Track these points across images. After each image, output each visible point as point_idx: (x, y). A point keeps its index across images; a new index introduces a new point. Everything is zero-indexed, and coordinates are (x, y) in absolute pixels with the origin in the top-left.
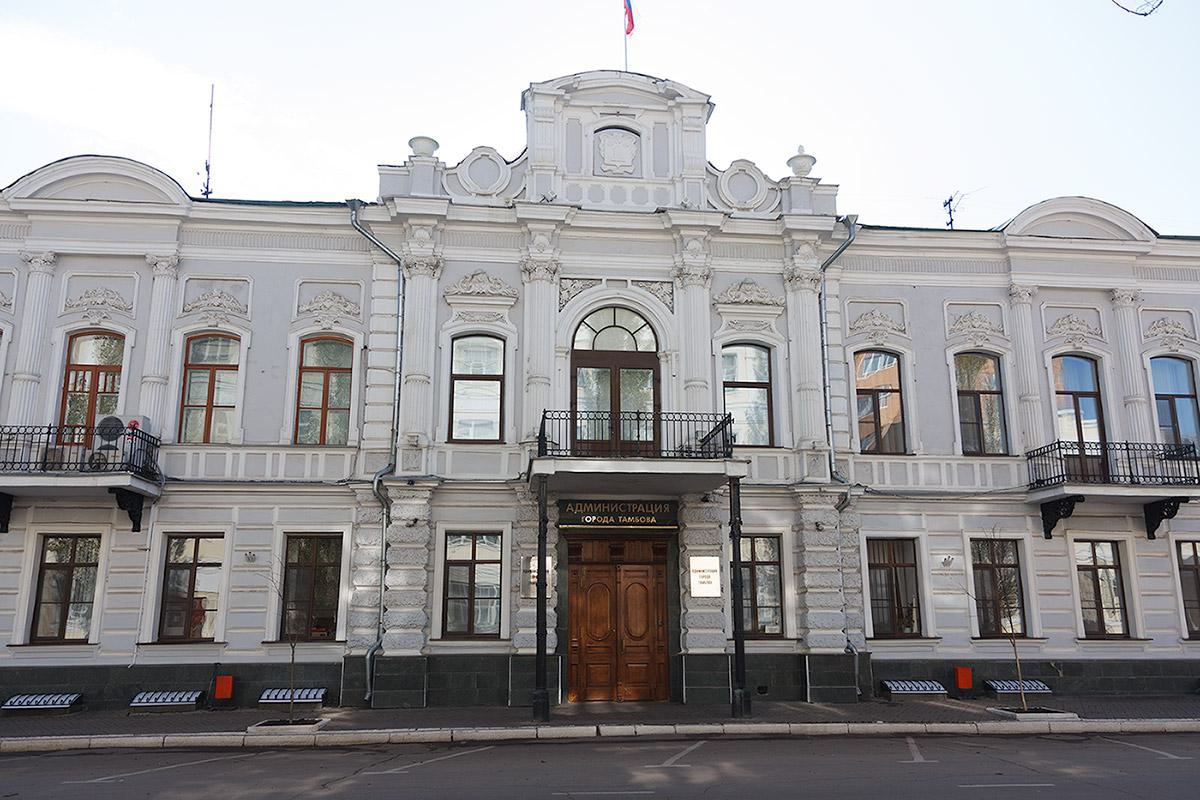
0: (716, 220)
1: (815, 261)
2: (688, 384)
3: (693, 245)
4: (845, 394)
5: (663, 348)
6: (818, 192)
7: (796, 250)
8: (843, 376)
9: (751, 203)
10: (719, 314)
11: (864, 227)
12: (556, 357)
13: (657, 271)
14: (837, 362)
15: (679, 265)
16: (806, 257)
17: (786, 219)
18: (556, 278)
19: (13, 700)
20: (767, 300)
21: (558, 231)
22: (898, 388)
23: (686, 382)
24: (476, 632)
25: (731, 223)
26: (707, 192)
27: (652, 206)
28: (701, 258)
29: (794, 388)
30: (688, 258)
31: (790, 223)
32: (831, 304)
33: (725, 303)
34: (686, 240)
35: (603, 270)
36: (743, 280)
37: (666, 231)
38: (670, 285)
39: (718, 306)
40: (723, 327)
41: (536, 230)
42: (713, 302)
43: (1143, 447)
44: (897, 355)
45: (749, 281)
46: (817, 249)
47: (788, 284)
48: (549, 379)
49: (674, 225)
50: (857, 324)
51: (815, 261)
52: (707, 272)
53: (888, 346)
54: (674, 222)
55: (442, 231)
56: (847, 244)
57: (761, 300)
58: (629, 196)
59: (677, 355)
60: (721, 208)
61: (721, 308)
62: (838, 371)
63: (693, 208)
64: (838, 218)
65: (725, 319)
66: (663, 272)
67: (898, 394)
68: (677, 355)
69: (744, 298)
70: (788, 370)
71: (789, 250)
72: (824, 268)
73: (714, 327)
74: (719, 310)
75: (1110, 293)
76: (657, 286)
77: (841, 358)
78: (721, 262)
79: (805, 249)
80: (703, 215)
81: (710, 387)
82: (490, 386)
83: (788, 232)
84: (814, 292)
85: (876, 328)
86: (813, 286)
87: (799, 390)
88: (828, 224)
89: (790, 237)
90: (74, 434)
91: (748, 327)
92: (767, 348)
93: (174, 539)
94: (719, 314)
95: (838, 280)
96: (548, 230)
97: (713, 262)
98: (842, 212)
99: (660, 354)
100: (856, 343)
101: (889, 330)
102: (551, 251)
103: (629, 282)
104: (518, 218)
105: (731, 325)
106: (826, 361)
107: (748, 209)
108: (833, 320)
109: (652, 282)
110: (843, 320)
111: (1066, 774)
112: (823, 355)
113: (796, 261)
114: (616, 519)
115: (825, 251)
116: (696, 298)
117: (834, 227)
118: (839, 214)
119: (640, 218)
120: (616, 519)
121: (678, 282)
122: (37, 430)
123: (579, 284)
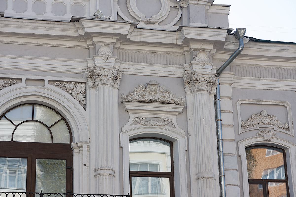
0: (123, 29)
1: (210, 67)
2: (98, 172)
3: (104, 50)
4: (238, 183)
5: (76, 139)
6: (213, 10)
7: (194, 57)
8: (236, 167)
9: (155, 18)
10: (127, 110)
11: (253, 40)
12: (168, 157)
13: (72, 73)
14: (230, 155)
15: (91, 67)
16: (203, 63)
17: (185, 30)
20: (169, 100)
21: (214, 52)
22: (169, 170)
23: (95, 170)
25: (137, 33)
26: (118, 8)
27: (68, 17)
28: (111, 62)
29: (193, 177)
30: (99, 61)
31: (188, 33)
32: (225, 105)
33: (132, 101)
34: (97, 46)
35: (24, 71)
36: (148, 81)
37: (80, 38)
38: (84, 85)
39: (126, 103)
40: (131, 122)
41: (100, 42)
42: (122, 100)
44: (283, 150)
45: (153, 82)
46: (212, 58)
47: (187, 86)
48: (114, 171)
49: (87, 33)
50: (249, 123)
51: (210, 67)
52: (115, 73)
53: (274, 141)
54: (87, 30)
55: (119, 48)
56: (237, 54)
57: (164, 99)
58: (49, 8)
59: (88, 147)
60: (127, 20)
61: (128, 106)
62: (232, 162)
63: (104, 19)
64: (229, 31)
65: (132, 116)
66: (77, 73)
67: (284, 184)
68: (88, 147)
69: (149, 97)
70: (188, 161)
71: (188, 57)
72: (219, 73)
73: (122, 122)
74: (127, 107)
76: (71, 86)
77: (235, 152)
78: (127, 66)
79: (201, 56)
80: (112, 24)
81: (117, 174)
82: (248, 190)
83: (187, 42)
84: (210, 93)
85: (264, 126)
86: (208, 88)
87: (197, 179)
88: (221, 36)
89: (189, 46)
91: (152, 123)
92: (170, 142)
94: (127, 110)
95: (231, 84)
96: (112, 43)
97: (123, 66)
98: (233, 25)
99: (73, 145)
100: (246, 139)
101: (276, 128)
102: (113, 61)
103: (47, 82)
104: (79, 35)
105: (137, 121)
106: (221, 153)
107: (153, 23)
108: (226, 118)
109: (67, 82)
110: (235, 118)
112: (218, 148)
113: (194, 66)
115: (219, 60)
117: (226, 39)
118: (230, 27)
121: (90, 82)
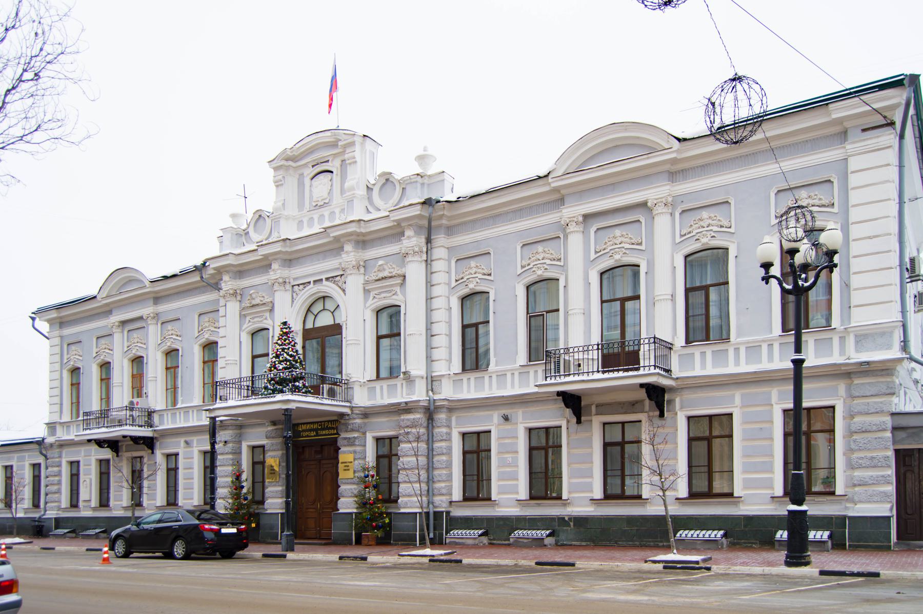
18: (288, 287)
19: (516, 532)
24: (714, 492)
43: (143, 410)
75: (644, 205)
90: (602, 349)
93: (168, 456)
111: (593, 601)
114: (317, 433)
116: (355, 282)
119: (250, 255)
120: (317, 433)
122: (576, 350)
123: (301, 287)
